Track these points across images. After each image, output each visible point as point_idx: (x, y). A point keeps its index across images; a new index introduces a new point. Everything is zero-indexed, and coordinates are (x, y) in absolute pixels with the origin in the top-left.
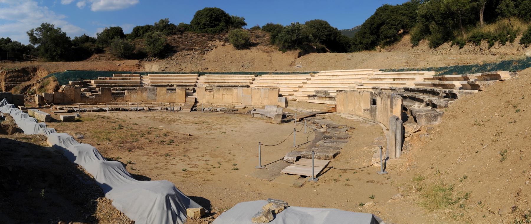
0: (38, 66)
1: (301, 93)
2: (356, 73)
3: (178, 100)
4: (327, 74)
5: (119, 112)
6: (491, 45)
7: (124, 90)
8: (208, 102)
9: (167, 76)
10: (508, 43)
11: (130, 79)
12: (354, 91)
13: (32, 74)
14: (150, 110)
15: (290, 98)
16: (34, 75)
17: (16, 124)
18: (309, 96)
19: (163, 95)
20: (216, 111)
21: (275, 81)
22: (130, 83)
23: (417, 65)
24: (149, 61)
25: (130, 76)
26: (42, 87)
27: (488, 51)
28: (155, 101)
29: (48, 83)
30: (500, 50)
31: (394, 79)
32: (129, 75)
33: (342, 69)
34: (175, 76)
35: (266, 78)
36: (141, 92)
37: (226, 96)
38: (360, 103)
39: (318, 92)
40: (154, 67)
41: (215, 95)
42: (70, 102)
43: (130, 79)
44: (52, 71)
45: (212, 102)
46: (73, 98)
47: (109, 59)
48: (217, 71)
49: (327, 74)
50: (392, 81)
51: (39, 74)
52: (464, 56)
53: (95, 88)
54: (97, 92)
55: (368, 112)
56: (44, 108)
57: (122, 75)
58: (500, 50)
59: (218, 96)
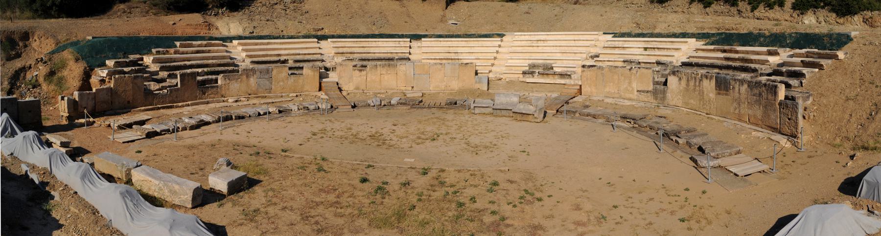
0: (30, 28)
1: (504, 68)
2: (576, 38)
3: (307, 88)
4: (523, 38)
5: (246, 125)
6: (753, 9)
7: (218, 73)
8: (357, 88)
9: (268, 44)
10: (776, 7)
11: (209, 52)
12: (616, 67)
13: (21, 44)
14: (280, 112)
15: (491, 75)
16: (26, 46)
17: (856, 206)
18: (524, 73)
19: (283, 81)
20: (390, 104)
21: (451, 50)
22: (213, 58)
23: (655, 27)
24: (215, 15)
25: (206, 46)
26: (52, 73)
27: (751, 15)
28: (270, 92)
29: (64, 65)
30: (767, 14)
31: (646, 49)
32: (205, 42)
33: (550, 31)
34: (281, 43)
35: (428, 44)
36: (247, 77)
37: (386, 77)
38: (630, 83)
39: (533, 66)
40: (232, 25)
41: (369, 75)
42: (126, 108)
43: (209, 52)
44: (62, 37)
45: (363, 87)
46: (131, 98)
47: (147, 12)
48: (339, 32)
49: (523, 38)
50: (641, 51)
51: (35, 45)
52: (709, 19)
53: (157, 73)
54: (163, 80)
55: (649, 94)
56: (82, 125)
57: (194, 43)
58: (767, 14)
59: (374, 78)
